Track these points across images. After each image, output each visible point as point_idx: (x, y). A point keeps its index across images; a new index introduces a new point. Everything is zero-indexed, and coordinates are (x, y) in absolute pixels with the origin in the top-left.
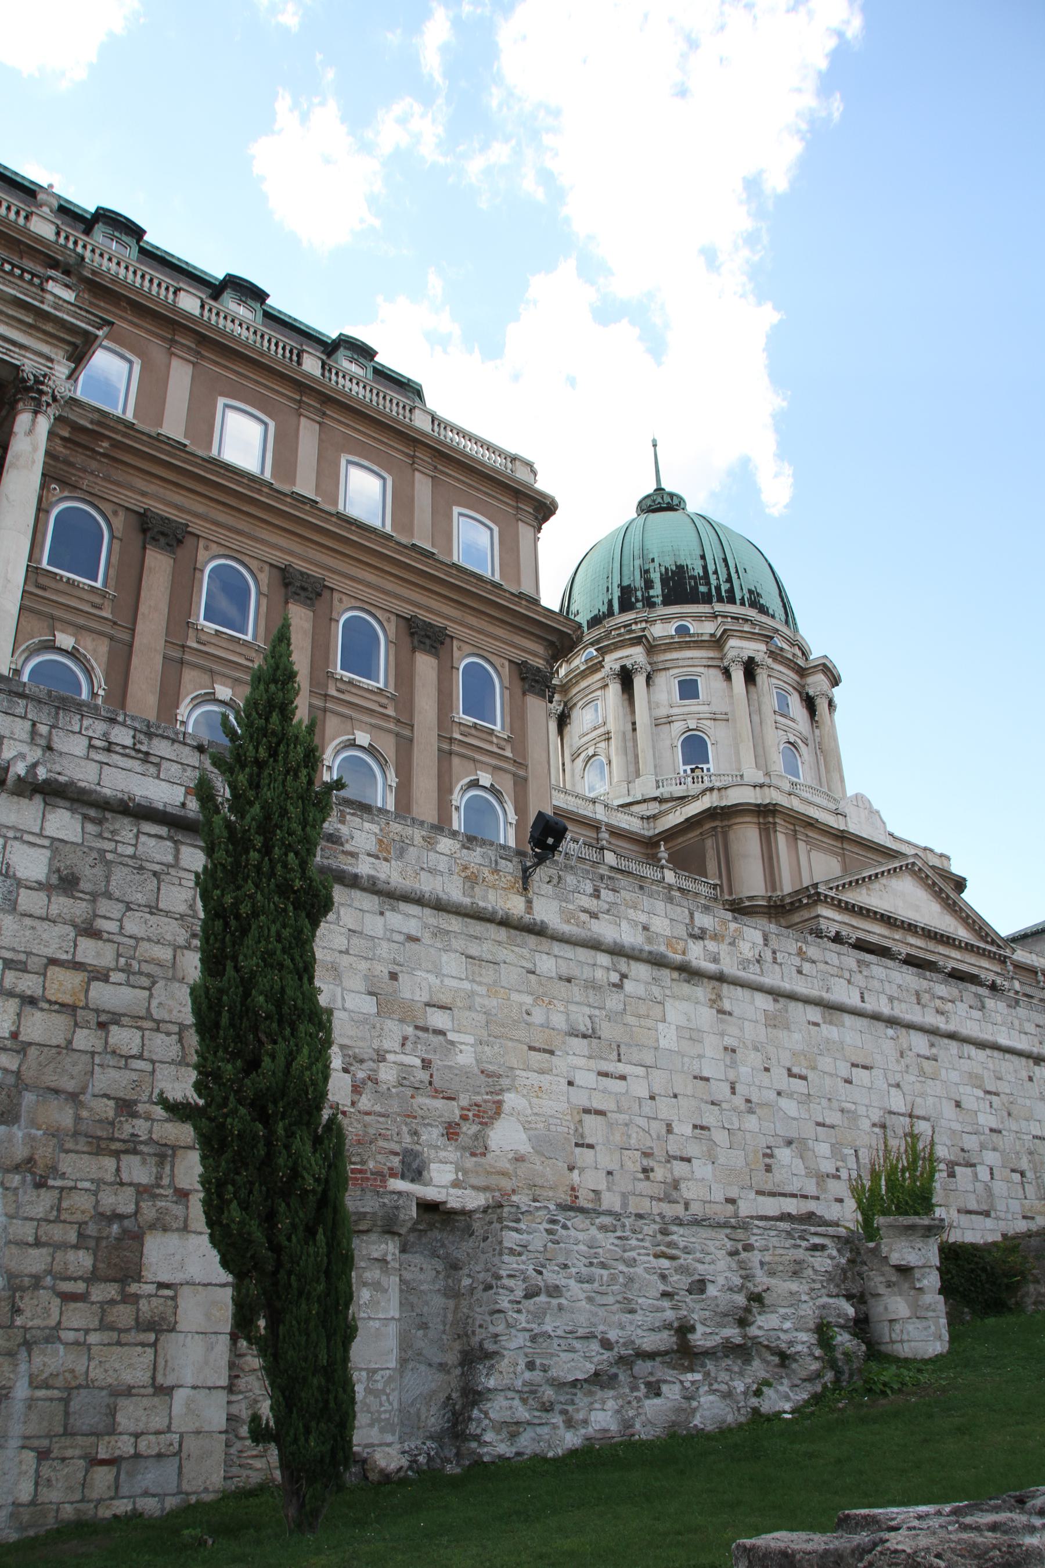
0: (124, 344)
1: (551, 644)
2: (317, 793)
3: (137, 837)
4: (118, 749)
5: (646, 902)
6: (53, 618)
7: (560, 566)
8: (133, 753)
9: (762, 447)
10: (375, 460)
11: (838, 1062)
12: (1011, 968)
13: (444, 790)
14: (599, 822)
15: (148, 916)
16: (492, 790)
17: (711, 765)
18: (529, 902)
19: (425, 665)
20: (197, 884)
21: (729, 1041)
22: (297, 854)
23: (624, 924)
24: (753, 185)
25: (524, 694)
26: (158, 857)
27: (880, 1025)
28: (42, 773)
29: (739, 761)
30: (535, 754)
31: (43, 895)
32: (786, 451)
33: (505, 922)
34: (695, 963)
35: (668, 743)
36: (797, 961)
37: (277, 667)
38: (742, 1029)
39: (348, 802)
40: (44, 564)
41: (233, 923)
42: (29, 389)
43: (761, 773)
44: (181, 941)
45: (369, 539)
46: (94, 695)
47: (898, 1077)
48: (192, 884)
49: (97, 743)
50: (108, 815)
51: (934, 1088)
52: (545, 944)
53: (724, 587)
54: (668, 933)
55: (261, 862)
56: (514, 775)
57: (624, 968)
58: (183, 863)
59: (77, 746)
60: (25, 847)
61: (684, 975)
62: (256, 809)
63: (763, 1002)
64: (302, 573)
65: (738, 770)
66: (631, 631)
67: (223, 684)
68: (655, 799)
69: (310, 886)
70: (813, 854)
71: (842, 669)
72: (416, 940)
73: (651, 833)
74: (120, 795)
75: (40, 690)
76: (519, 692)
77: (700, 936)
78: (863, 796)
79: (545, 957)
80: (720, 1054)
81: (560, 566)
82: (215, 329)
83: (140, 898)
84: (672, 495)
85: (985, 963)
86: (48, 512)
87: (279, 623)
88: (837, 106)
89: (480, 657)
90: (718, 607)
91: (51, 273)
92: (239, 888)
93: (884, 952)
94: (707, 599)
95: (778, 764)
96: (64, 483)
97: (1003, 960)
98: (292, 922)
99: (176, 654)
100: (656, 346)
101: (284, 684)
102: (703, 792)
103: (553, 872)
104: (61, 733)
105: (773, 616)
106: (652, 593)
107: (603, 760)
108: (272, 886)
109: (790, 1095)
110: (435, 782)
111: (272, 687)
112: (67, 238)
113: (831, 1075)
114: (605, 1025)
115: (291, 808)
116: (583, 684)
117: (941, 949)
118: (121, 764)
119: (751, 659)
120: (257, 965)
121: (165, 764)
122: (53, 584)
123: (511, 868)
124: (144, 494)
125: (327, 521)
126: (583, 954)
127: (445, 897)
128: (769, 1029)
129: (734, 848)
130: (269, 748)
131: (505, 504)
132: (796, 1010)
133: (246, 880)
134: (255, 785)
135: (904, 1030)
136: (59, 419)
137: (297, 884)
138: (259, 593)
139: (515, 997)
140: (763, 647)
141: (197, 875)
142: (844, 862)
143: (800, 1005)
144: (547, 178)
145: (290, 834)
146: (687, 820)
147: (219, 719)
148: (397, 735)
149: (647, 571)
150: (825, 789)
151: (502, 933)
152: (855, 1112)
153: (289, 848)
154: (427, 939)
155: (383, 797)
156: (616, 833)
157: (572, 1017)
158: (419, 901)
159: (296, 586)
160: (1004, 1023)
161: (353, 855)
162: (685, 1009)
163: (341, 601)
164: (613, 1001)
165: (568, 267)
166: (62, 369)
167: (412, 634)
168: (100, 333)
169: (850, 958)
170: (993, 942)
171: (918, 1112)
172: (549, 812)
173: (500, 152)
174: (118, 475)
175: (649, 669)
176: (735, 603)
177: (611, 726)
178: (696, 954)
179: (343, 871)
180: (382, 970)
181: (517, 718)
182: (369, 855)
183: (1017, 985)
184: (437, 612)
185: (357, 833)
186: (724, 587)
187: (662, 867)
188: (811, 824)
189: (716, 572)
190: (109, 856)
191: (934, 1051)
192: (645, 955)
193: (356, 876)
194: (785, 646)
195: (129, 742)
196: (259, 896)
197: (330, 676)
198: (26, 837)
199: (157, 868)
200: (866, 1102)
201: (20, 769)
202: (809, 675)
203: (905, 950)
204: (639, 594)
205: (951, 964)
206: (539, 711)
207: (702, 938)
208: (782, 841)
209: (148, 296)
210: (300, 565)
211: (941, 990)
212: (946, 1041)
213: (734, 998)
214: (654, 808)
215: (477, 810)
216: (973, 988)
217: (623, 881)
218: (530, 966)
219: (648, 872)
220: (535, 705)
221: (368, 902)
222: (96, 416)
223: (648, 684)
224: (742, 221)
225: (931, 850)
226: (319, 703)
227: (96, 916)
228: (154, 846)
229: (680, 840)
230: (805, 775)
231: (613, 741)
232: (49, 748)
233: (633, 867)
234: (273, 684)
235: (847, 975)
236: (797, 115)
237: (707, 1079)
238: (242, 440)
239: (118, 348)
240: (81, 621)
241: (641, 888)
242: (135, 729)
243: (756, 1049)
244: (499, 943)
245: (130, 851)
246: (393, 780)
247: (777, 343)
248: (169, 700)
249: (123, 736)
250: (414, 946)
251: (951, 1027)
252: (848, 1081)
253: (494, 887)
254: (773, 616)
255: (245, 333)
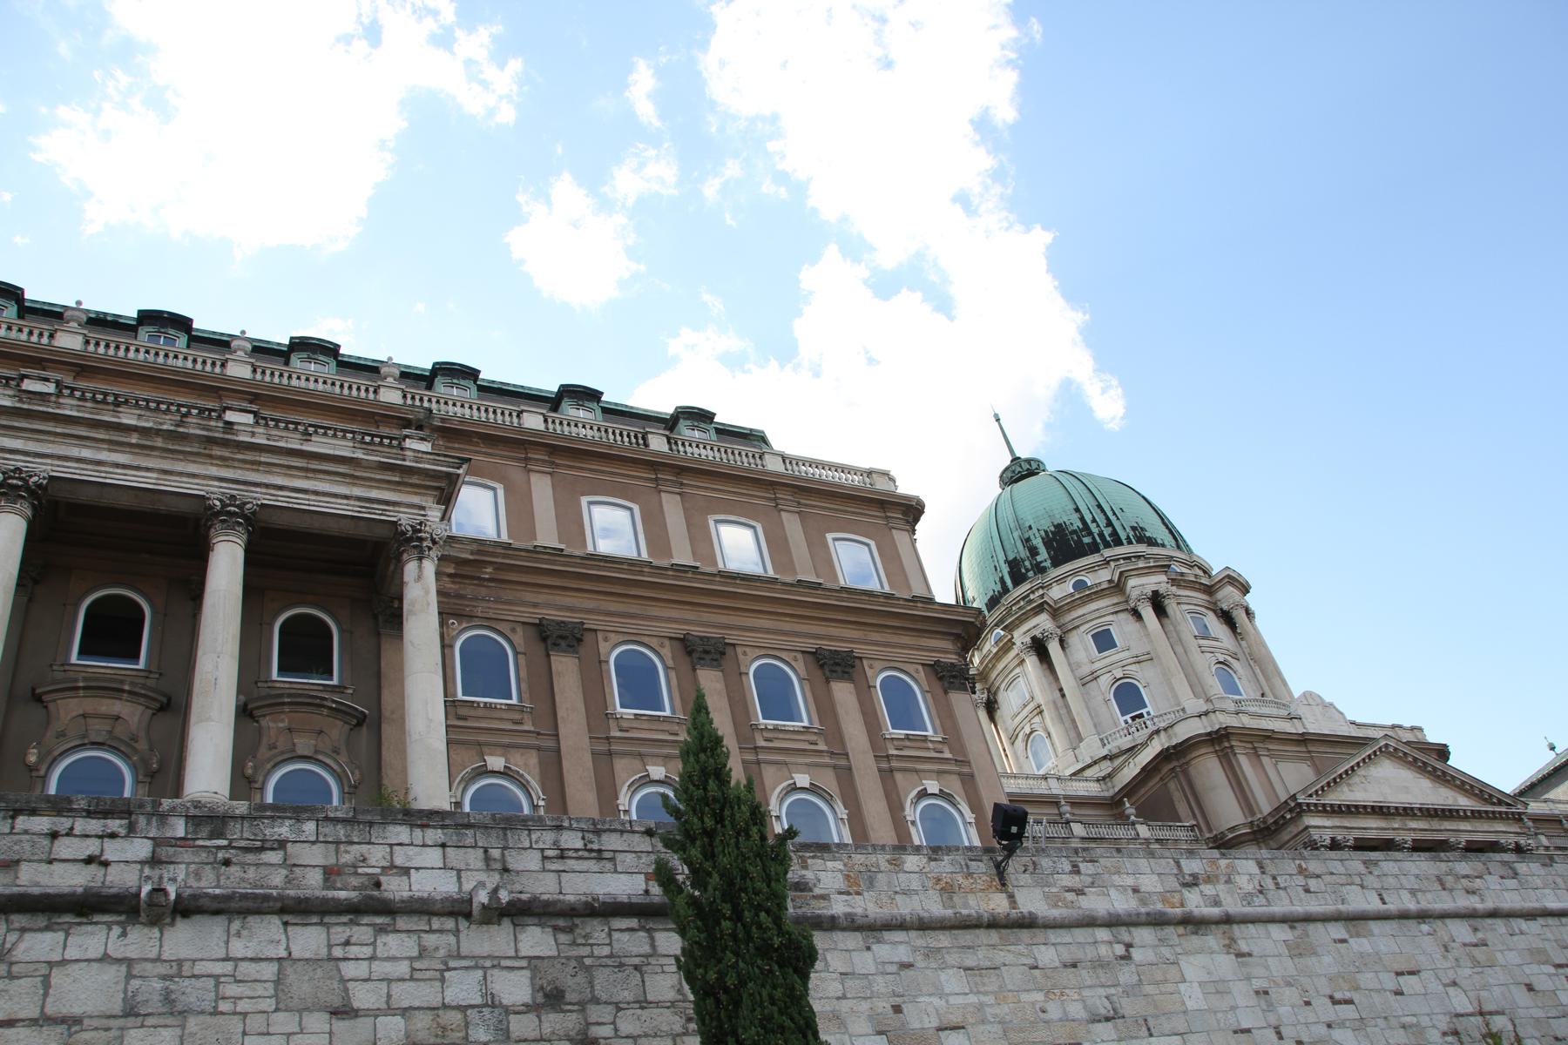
0: (484, 476)
1: (958, 636)
2: (772, 847)
3: (610, 935)
4: (570, 853)
5: (1128, 864)
6: (479, 744)
7: (947, 559)
8: (586, 854)
9: (1080, 365)
10: (741, 513)
11: (1381, 975)
12: (1530, 824)
13: (896, 808)
14: (1057, 796)
15: (639, 1012)
16: (942, 795)
17: (1149, 708)
18: (1011, 897)
19: (843, 692)
20: (679, 968)
21: (1258, 984)
22: (768, 912)
23: (1112, 892)
24: (983, 125)
25: (946, 692)
26: (635, 951)
27: (1412, 923)
28: (504, 896)
29: (1176, 696)
30: (973, 749)
31: (532, 1016)
32: (1104, 364)
33: (994, 924)
34: (1196, 912)
35: (1100, 698)
36: (1300, 880)
37: (702, 737)
38: (1267, 968)
39: (805, 847)
40: (460, 696)
41: (723, 997)
42: (411, 539)
43: (1201, 701)
44: (678, 1028)
45: (757, 588)
46: (535, 807)
47: (1451, 975)
48: (674, 968)
49: (549, 853)
50: (577, 921)
51: (1495, 976)
52: (1040, 935)
53: (1107, 532)
54: (1160, 889)
55: (735, 930)
56: (959, 774)
57: (1127, 938)
58: (661, 950)
59: (531, 861)
60: (505, 973)
61: (1189, 928)
62: (715, 879)
63: (1279, 933)
64: (701, 638)
65: (1179, 703)
66: (1031, 601)
67: (655, 764)
68: (1105, 758)
69: (790, 940)
70: (1281, 766)
71: (1247, 574)
72: (909, 966)
73: (1111, 793)
74: (583, 898)
75: (484, 816)
76: (939, 691)
77: (1193, 882)
78: (1311, 693)
79: (1043, 948)
80: (1253, 1000)
81: (947, 559)
82: (563, 437)
83: (627, 995)
84: (1028, 461)
85: (1500, 826)
86: (452, 647)
87: (694, 695)
88: (1036, 27)
89: (892, 668)
90: (1107, 553)
91: (406, 432)
92: (720, 961)
93: (1387, 845)
94: (1094, 548)
95: (1215, 687)
96: (460, 616)
97: (1518, 818)
98: (781, 981)
99: (603, 747)
100: (943, 305)
101: (713, 750)
102: (1151, 737)
103: (1026, 860)
104: (514, 853)
105: (1163, 545)
106: (1039, 558)
107: (1039, 736)
108: (752, 950)
109: (1342, 1024)
110: (884, 804)
111: (702, 756)
112: (413, 398)
113: (1378, 991)
114: (1125, 1001)
115: (751, 869)
116: (1000, 666)
117: (1447, 825)
118: (577, 868)
119: (1155, 593)
120: (758, 1034)
121: (619, 857)
122: (472, 713)
123: (982, 867)
124: (535, 605)
125: (711, 582)
126: (1081, 934)
127: (926, 915)
128: (1296, 960)
129: (1199, 783)
130: (714, 815)
131: (874, 517)
132: (1317, 932)
133: (723, 951)
134: (709, 855)
135: (1439, 923)
136: (442, 559)
137: (777, 941)
138: (666, 668)
139: (1025, 997)
140: (1163, 578)
141: (677, 959)
142: (1314, 766)
143: (1319, 925)
144: (782, 178)
145: (756, 894)
146: (1143, 769)
147: (659, 801)
148: (835, 767)
149: (1028, 540)
150: (1271, 698)
151: (994, 936)
152: (1417, 1025)
153: (760, 908)
154: (920, 963)
155: (838, 832)
156: (1078, 802)
157: (1089, 1002)
158: (901, 925)
159: (700, 652)
160: (1539, 885)
161: (824, 897)
162: (1200, 964)
163: (745, 653)
164: (1126, 975)
165: (832, 252)
166: (434, 514)
167: (822, 666)
168: (460, 471)
169: (1356, 862)
170: (1500, 802)
171: (1487, 1007)
172: (1004, 801)
173: (732, 169)
174: (508, 595)
175: (1059, 632)
176: (1121, 544)
177: (1040, 699)
178: (1195, 902)
179: (819, 916)
180: (884, 1006)
181: (947, 718)
182: (840, 893)
183: (1544, 840)
184: (839, 638)
185: (822, 875)
186: (1107, 532)
187: (1133, 824)
188: (1268, 736)
189: (1094, 520)
190: (588, 961)
191: (1480, 935)
192: (1143, 918)
193: (833, 918)
194: (1184, 570)
195: (579, 844)
196: (741, 964)
197: (754, 728)
198: (504, 963)
199: (637, 961)
200: (1427, 1010)
201: (482, 897)
202: (1216, 591)
203: (1410, 837)
204: (1027, 563)
205: (1464, 838)
206: (964, 704)
207: (1196, 885)
208: (1244, 762)
209: (496, 426)
210: (697, 631)
211: (1463, 867)
212: (1489, 921)
213: (1249, 937)
214: (1106, 767)
215: (937, 821)
216: (1497, 857)
217: (1099, 850)
218: (1030, 961)
219: (1120, 832)
220: (959, 700)
221: (852, 940)
222: (475, 547)
223: (1063, 648)
224: (983, 161)
225: (1400, 727)
226: (750, 757)
227: (589, 1024)
228: (629, 940)
229: (1143, 791)
230: (1247, 690)
231: (1046, 713)
232: (506, 870)
233: (1104, 832)
234: (703, 756)
235: (1357, 880)
236: (1003, 47)
237: (1248, 1031)
238: (612, 529)
239: (480, 480)
240: (506, 740)
241: (1119, 850)
242: (582, 830)
243: (1289, 984)
244: (993, 946)
245: (606, 951)
246: (843, 812)
247: (1057, 261)
248: (607, 793)
249: (572, 840)
250: (910, 972)
251: (1490, 904)
252: (1399, 993)
253: (972, 891)
254: (1163, 545)
255: (590, 433)
